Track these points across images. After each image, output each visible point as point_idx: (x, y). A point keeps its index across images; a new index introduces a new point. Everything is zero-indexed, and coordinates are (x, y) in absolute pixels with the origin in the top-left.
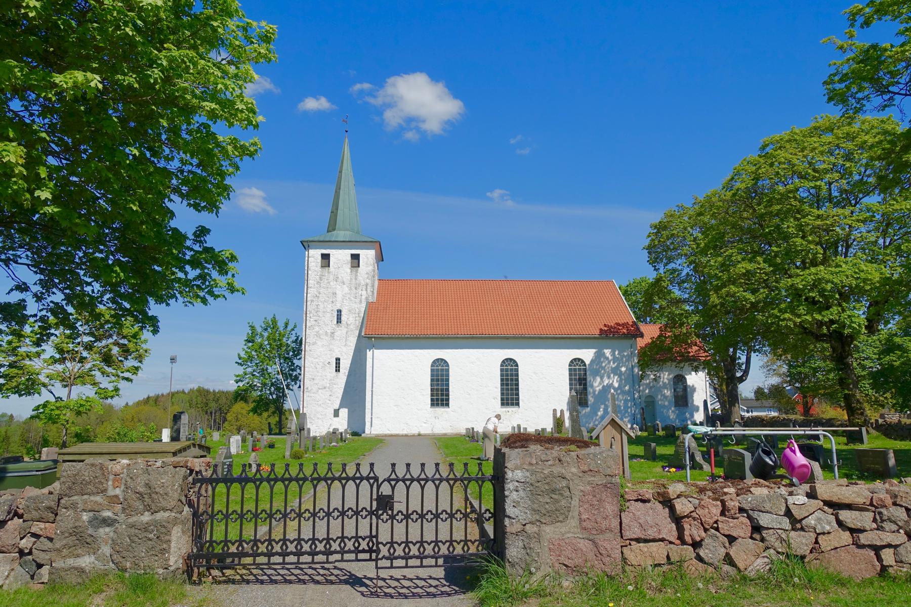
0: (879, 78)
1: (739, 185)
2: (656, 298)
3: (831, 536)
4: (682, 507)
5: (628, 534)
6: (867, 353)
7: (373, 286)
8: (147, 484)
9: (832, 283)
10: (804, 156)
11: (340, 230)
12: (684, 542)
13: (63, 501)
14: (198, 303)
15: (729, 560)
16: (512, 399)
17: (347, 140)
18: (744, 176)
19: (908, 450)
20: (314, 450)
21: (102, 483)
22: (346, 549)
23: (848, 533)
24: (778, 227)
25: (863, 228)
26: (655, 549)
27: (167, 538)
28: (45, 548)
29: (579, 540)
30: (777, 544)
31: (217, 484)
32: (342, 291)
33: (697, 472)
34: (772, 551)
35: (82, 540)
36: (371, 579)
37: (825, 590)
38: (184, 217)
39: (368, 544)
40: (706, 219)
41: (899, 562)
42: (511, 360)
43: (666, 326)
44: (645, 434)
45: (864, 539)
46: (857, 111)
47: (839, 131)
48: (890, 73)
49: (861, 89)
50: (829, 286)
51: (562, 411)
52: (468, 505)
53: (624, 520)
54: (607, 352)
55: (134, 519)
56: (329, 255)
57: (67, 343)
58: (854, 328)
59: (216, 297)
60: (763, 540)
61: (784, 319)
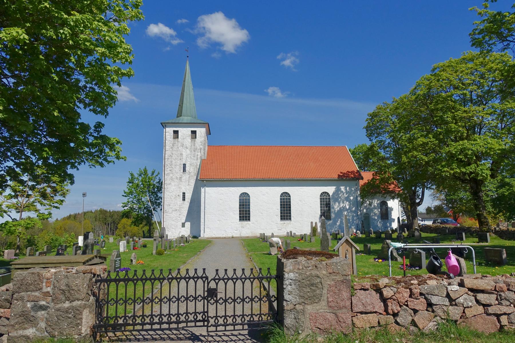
0: (501, 33)
1: (419, 92)
2: (371, 157)
3: (472, 309)
4: (387, 293)
5: (356, 309)
6: (490, 189)
7: (204, 150)
8: (67, 285)
9: (472, 150)
10: (458, 76)
11: (184, 116)
12: (388, 314)
13: (15, 296)
14: (98, 167)
15: (414, 323)
16: (287, 216)
17: (188, 62)
18: (422, 87)
19: (513, 247)
20: (170, 249)
21: (39, 285)
22: (189, 320)
23: (482, 307)
24: (441, 117)
25: (490, 118)
26: (371, 318)
27: (80, 316)
28: (5, 324)
29: (327, 314)
30: (441, 314)
31: (110, 283)
32: (186, 153)
33: (394, 262)
34: (438, 318)
35: (27, 319)
36: (204, 336)
37: (468, 341)
38: (87, 117)
39: (202, 317)
40: (400, 111)
41: (510, 323)
42: (286, 193)
43: (376, 173)
44: (364, 236)
45: (491, 310)
46: (489, 51)
47: (477, 61)
48: (508, 29)
49: (491, 38)
50: (470, 152)
51: (316, 223)
52: (262, 286)
53: (354, 301)
54: (343, 188)
55: (60, 305)
56: (178, 131)
57: (19, 186)
58: (483, 176)
59: (109, 162)
60: (433, 311)
61: (444, 171)
